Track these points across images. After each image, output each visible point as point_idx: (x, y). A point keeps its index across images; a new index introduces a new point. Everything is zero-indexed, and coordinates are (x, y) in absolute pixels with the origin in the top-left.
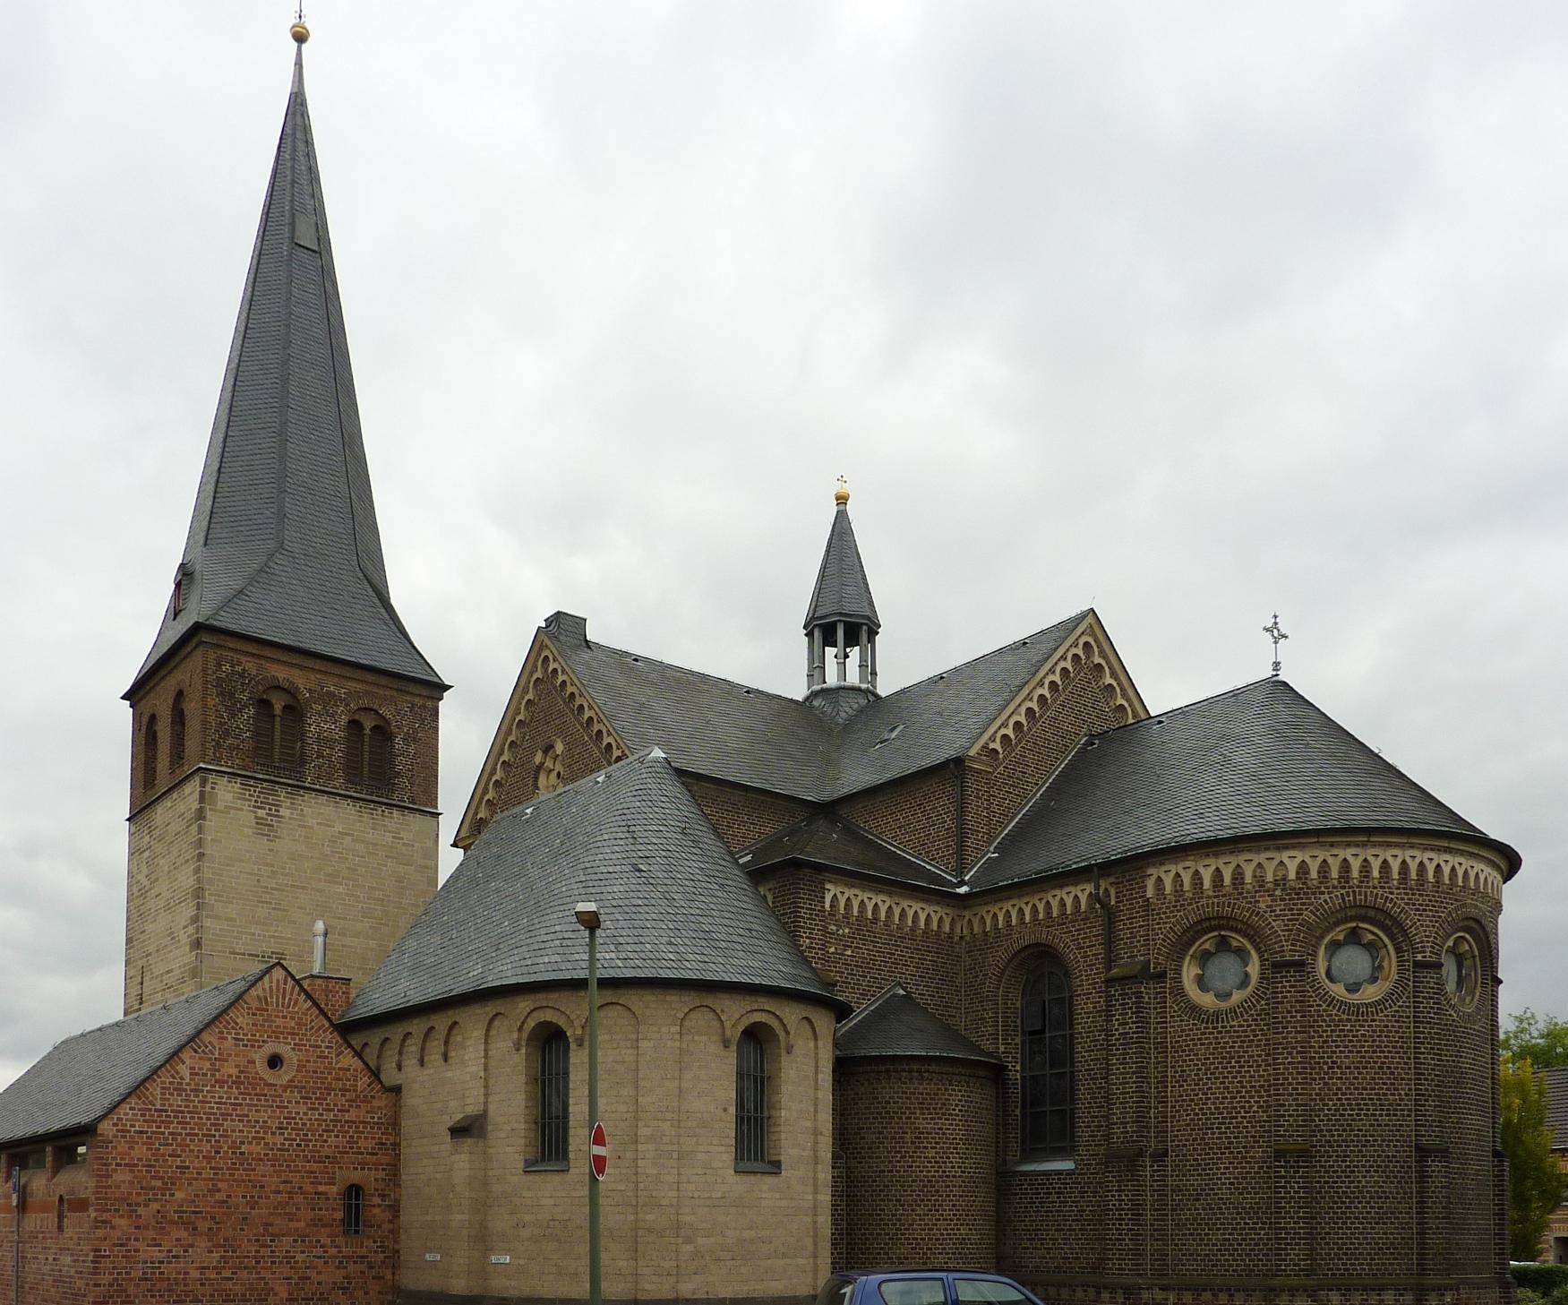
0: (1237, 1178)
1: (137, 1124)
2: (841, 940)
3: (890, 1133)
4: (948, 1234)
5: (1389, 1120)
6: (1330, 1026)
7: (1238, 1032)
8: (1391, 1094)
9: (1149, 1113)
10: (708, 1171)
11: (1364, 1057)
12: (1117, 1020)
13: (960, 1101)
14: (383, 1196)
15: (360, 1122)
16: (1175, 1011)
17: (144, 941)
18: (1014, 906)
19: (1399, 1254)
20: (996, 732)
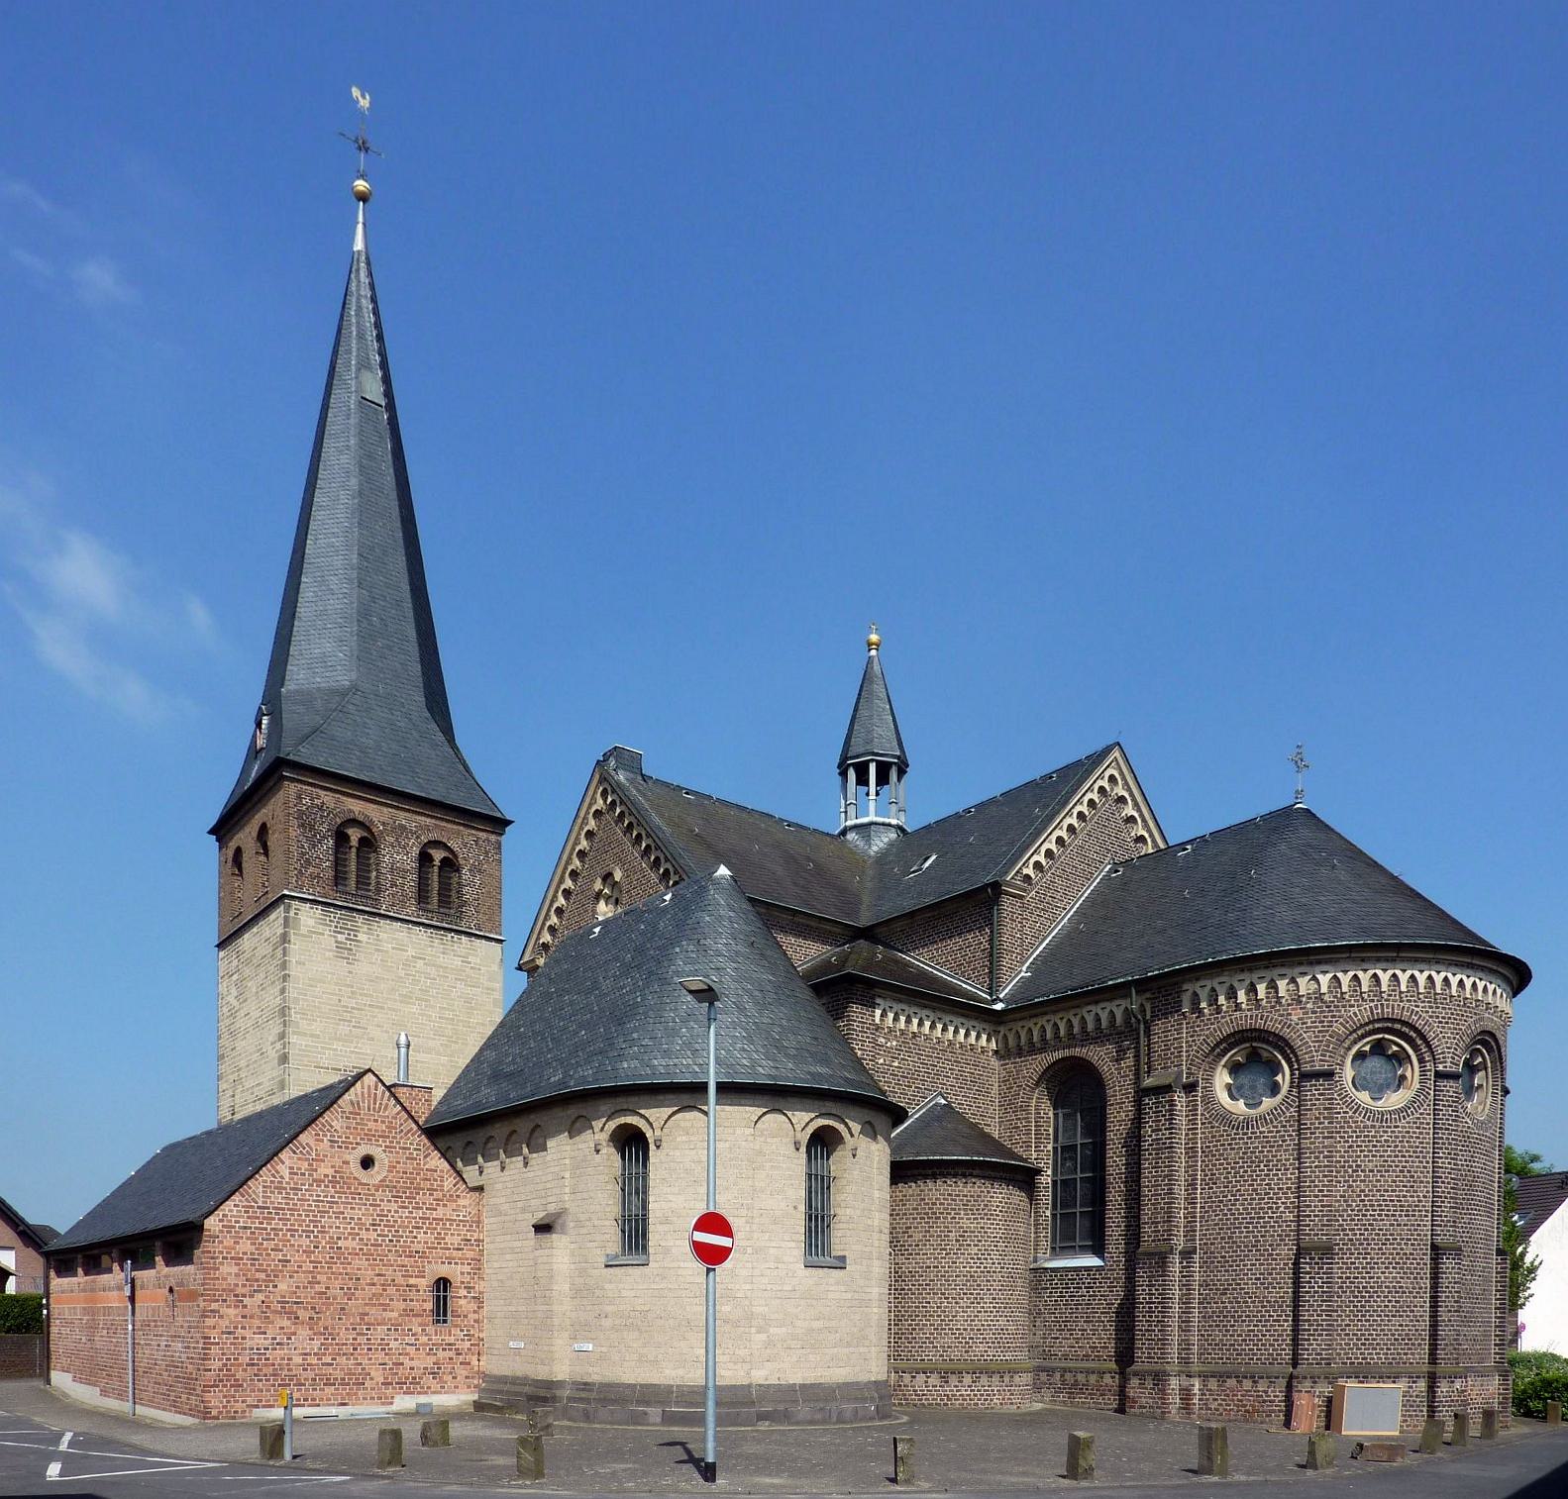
0: (1263, 1274)
1: (241, 1220)
2: (889, 1052)
3: (936, 1232)
4: (988, 1325)
5: (1408, 1220)
6: (1356, 1132)
7: (1267, 1137)
8: (1411, 1196)
9: (1179, 1213)
10: (780, 1266)
11: (1387, 1161)
12: (1150, 1127)
13: (1001, 1202)
14: (469, 1288)
15: (447, 1220)
16: (1206, 1119)
17: (234, 1057)
18: (1048, 1021)
19: (1413, 1344)
20: (1029, 858)
